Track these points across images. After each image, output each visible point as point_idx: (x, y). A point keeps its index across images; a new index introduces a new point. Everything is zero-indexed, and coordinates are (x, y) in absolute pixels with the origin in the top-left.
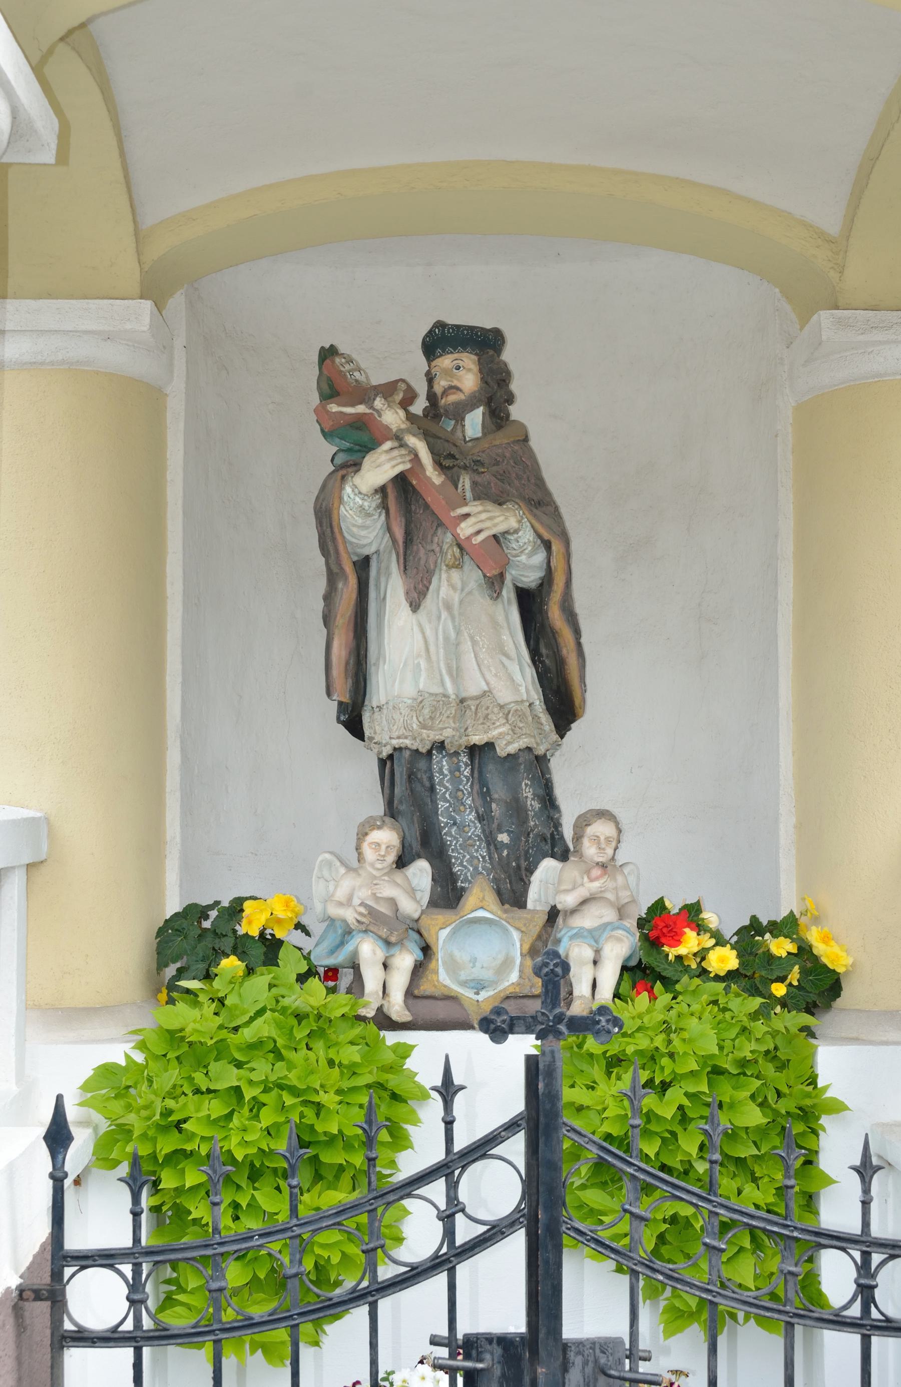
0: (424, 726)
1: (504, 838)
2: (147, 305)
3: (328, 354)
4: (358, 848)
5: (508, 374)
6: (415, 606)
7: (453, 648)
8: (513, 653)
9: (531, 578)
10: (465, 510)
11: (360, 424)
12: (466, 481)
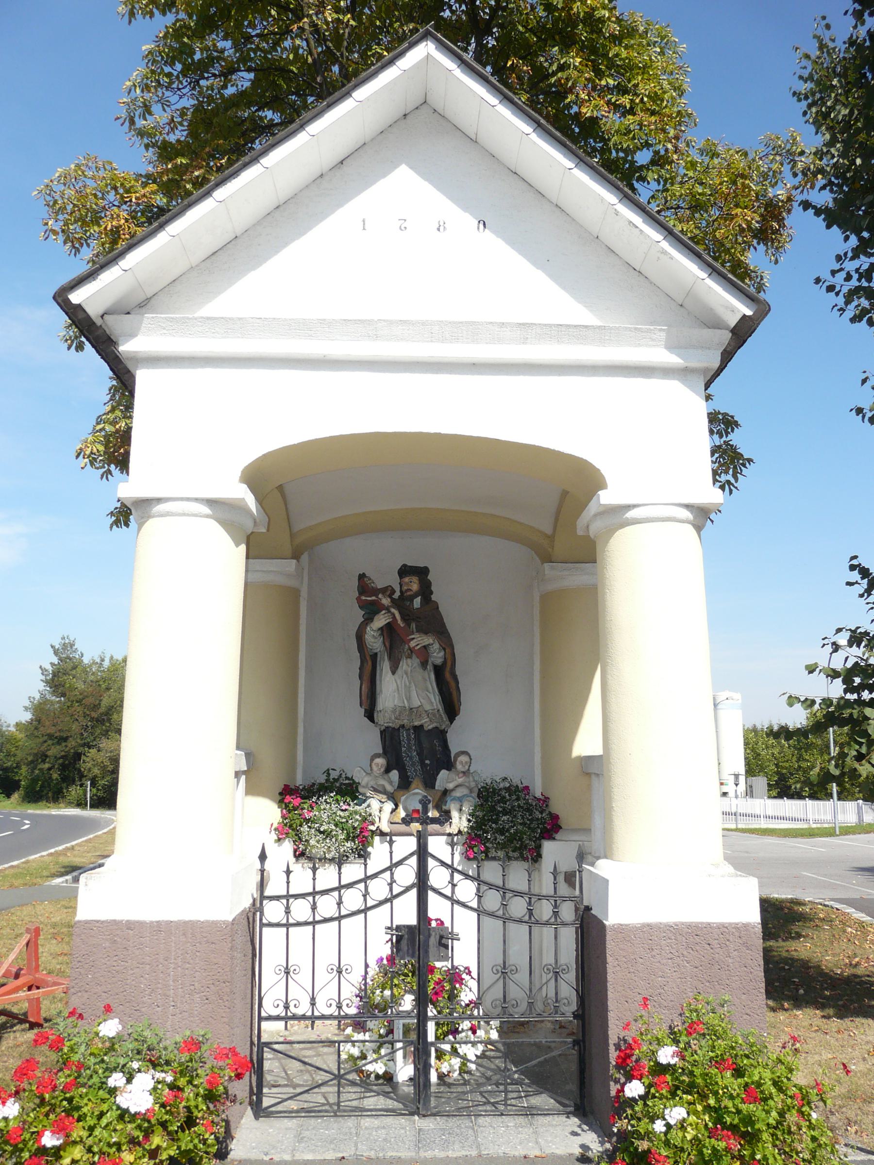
0: (396, 718)
1: (427, 762)
2: (294, 561)
3: (362, 577)
4: (371, 765)
5: (430, 583)
6: (393, 673)
7: (408, 689)
8: (431, 690)
9: (439, 662)
10: (413, 636)
11: (373, 603)
12: (413, 625)
